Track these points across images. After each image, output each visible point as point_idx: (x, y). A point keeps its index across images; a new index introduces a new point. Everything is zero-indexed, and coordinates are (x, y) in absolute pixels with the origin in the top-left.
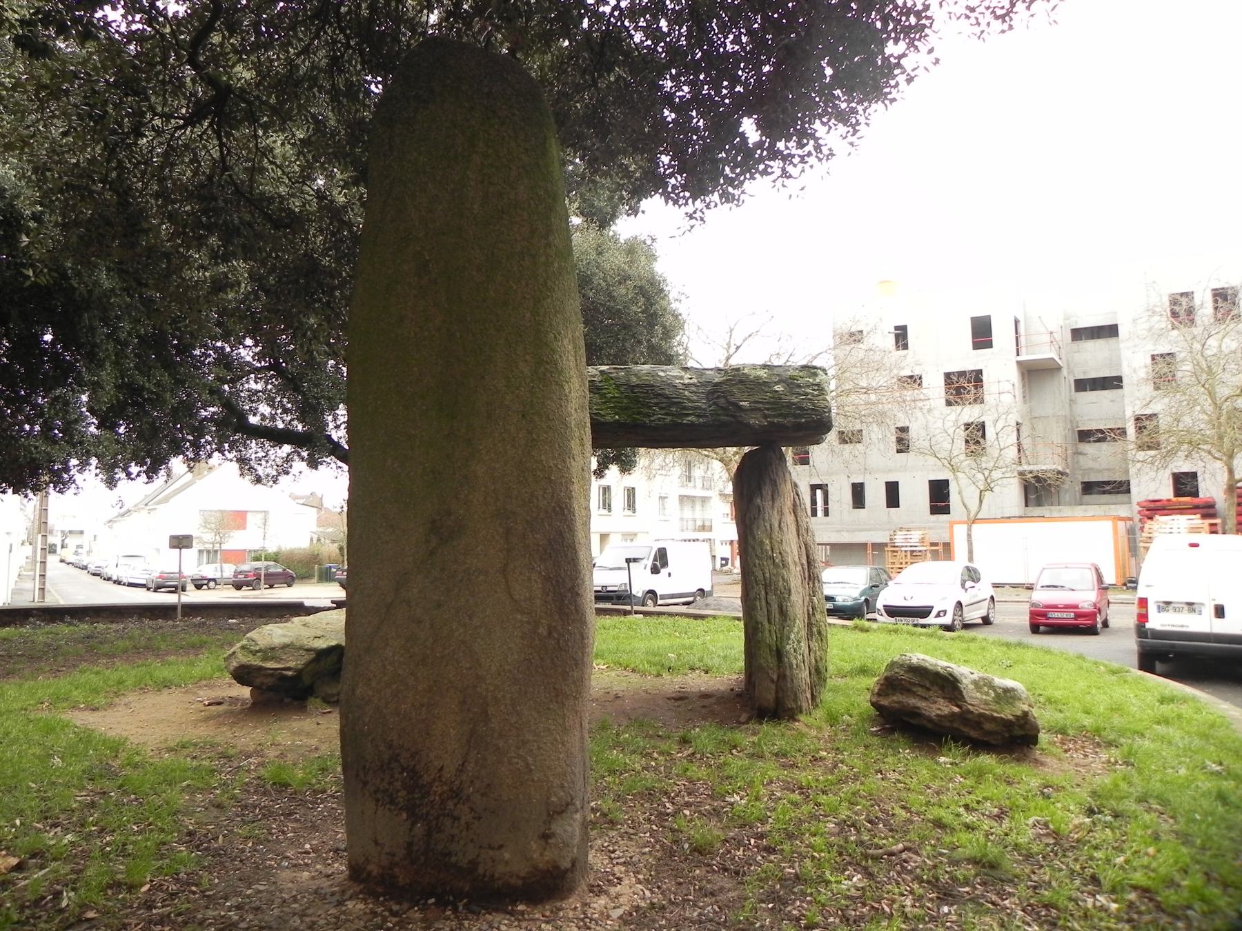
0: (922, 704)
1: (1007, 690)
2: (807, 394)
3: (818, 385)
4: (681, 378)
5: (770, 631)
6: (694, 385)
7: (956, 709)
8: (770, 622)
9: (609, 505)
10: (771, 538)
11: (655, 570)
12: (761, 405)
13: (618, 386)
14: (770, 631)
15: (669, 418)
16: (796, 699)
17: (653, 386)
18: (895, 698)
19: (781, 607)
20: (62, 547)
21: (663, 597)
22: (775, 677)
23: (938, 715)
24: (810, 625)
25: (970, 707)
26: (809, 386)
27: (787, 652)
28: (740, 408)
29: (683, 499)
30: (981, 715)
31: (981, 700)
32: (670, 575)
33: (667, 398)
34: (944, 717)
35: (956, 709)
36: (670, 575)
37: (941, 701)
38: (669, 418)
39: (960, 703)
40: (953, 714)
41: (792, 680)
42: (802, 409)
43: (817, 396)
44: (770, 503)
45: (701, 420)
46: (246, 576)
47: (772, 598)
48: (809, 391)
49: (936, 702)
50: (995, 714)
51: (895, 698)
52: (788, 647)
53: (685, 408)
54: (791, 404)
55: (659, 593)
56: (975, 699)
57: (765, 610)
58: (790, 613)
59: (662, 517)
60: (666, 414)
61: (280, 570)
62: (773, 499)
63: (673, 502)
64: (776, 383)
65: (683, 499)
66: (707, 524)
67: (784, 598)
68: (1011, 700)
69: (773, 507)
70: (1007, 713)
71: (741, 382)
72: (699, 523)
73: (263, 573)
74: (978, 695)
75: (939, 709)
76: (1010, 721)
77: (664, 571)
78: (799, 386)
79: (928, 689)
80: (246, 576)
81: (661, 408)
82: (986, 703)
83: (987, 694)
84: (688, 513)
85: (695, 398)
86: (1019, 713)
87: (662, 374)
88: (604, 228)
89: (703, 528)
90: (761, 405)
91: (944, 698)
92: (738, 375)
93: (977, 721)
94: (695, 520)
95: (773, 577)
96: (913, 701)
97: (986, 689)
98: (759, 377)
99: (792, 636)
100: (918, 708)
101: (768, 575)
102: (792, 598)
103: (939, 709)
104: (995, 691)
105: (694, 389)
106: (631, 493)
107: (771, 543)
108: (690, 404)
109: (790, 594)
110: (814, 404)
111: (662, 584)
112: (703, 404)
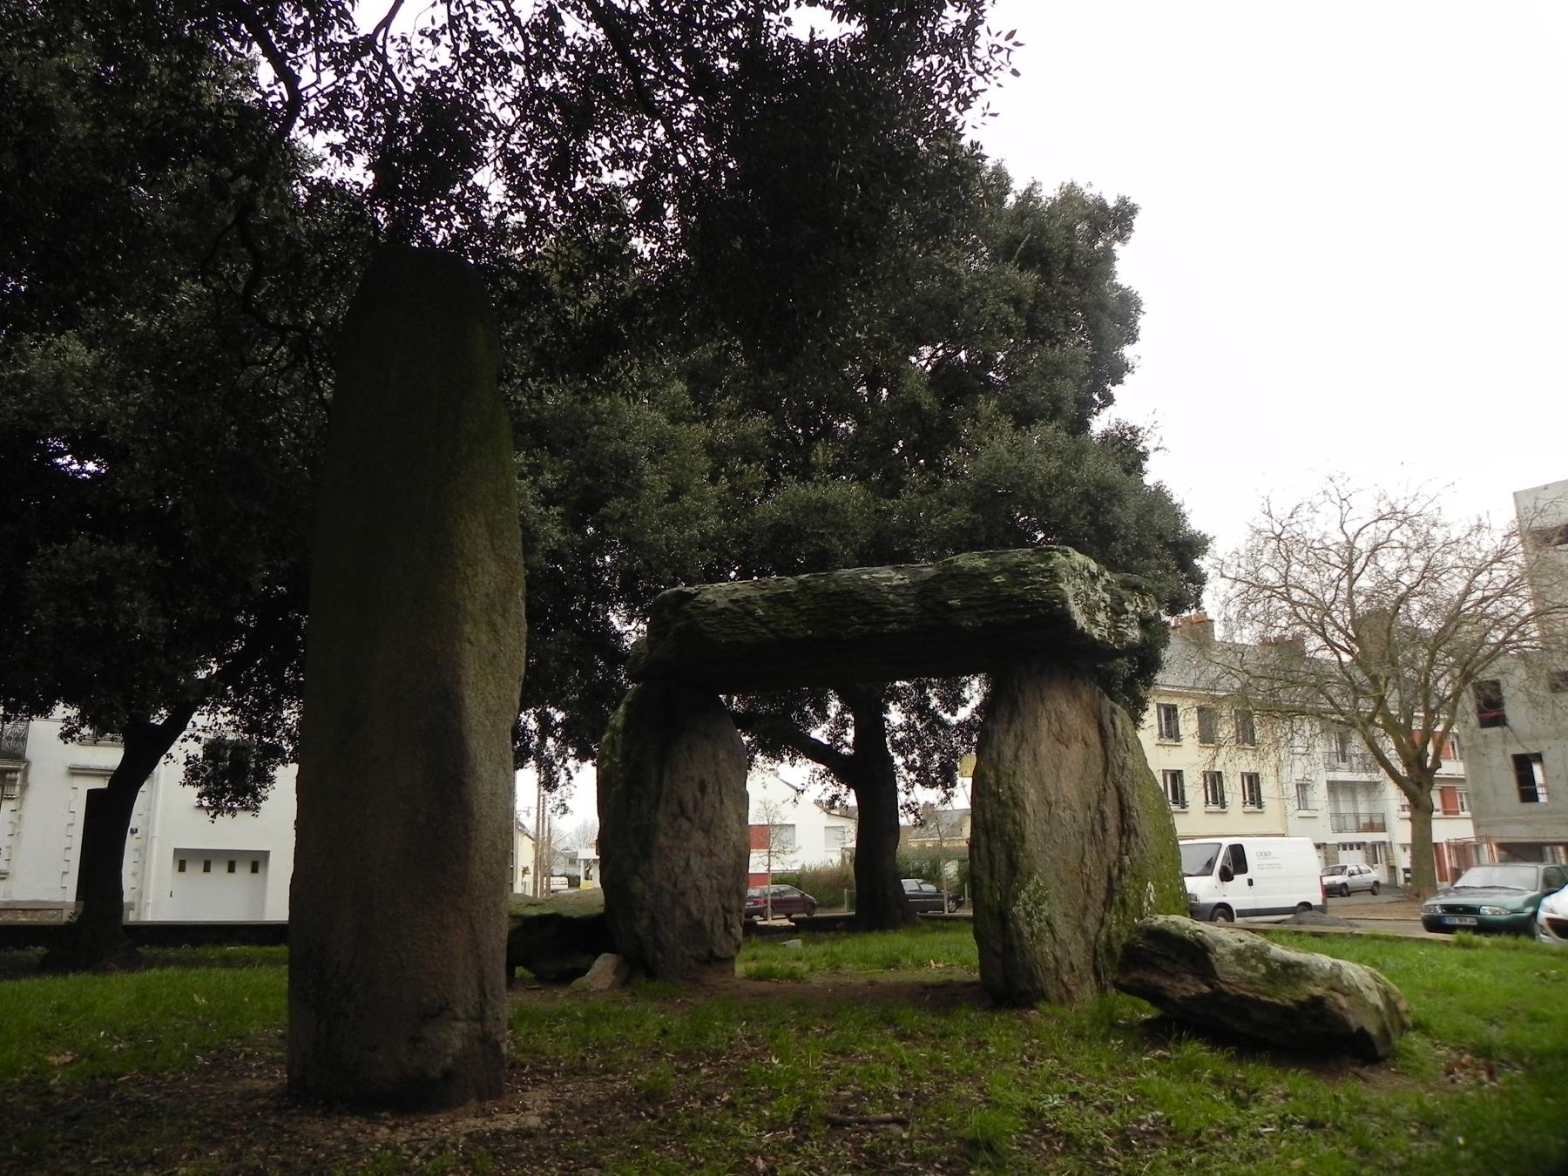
0: (1166, 983)
1: (1287, 965)
2: (1034, 583)
3: (1051, 570)
4: (890, 579)
5: (991, 888)
6: (904, 586)
7: (1206, 989)
8: (992, 876)
9: (1223, 798)
10: (997, 770)
11: (1226, 876)
12: (975, 603)
13: (815, 596)
14: (991, 888)
15: (867, 628)
16: (1032, 978)
17: (852, 592)
18: (1135, 975)
19: (1009, 857)
20: (586, 879)
21: (1242, 913)
22: (998, 948)
23: (1183, 998)
24: (1110, 891)
25: (1223, 986)
26: (1038, 574)
27: (1014, 916)
28: (951, 609)
29: (1333, 786)
30: (1241, 998)
31: (1242, 977)
32: (1250, 882)
33: (867, 603)
34: (1191, 999)
35: (1206, 989)
36: (1250, 882)
37: (1189, 977)
38: (867, 628)
39: (1212, 980)
40: (1202, 996)
41: (1023, 953)
42: (1026, 602)
43: (1047, 583)
44: (1005, 726)
45: (904, 627)
46: (756, 903)
47: (997, 846)
48: (1038, 579)
49: (1182, 980)
50: (1264, 998)
51: (1135, 975)
52: (1014, 909)
53: (888, 614)
54: (1011, 597)
55: (1235, 908)
56: (1229, 972)
57: (987, 864)
58: (1024, 863)
59: (1305, 813)
60: (865, 624)
61: (797, 895)
62: (1010, 721)
63: (1319, 795)
64: (996, 574)
65: (1333, 786)
66: (1377, 821)
67: (1015, 846)
68: (1294, 980)
69: (1008, 731)
70: (1285, 997)
71: (953, 576)
72: (1364, 820)
73: (769, 898)
74: (1239, 970)
75: (1185, 989)
76: (1288, 1008)
77: (1240, 879)
78: (1026, 574)
79: (1175, 962)
80: (756, 903)
81: (859, 617)
82: (1250, 981)
83: (1254, 969)
84: (1345, 807)
85: (901, 601)
86: (1304, 998)
87: (866, 577)
88: (1078, 433)
89: (1371, 827)
90: (975, 603)
91: (1194, 974)
92: (950, 568)
93: (1241, 1006)
94: (1357, 816)
95: (996, 818)
96: (1155, 979)
97: (1253, 962)
98: (976, 568)
99: (1024, 895)
100: (1162, 988)
101: (988, 816)
102: (1027, 846)
103: (1185, 989)
104: (1267, 965)
105: (902, 591)
106: (1252, 782)
107: (997, 775)
108: (893, 610)
109: (1023, 842)
110: (1041, 595)
111: (1237, 894)
112: (910, 608)
